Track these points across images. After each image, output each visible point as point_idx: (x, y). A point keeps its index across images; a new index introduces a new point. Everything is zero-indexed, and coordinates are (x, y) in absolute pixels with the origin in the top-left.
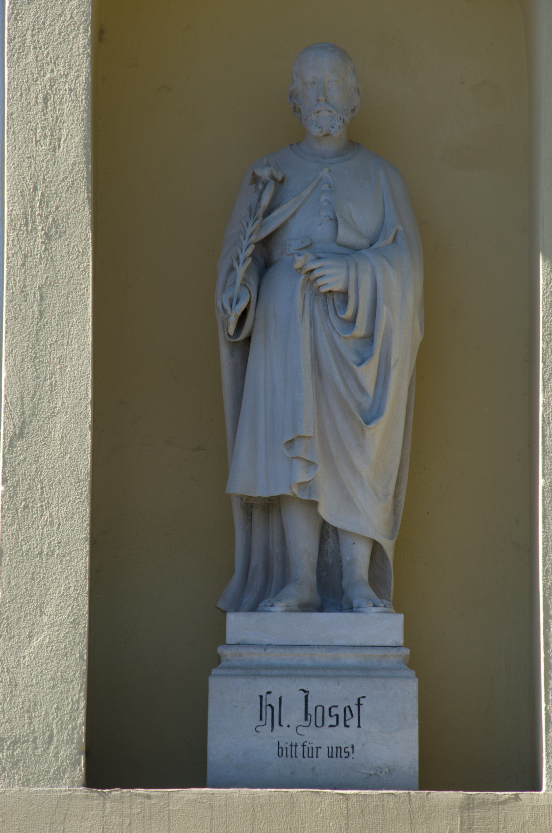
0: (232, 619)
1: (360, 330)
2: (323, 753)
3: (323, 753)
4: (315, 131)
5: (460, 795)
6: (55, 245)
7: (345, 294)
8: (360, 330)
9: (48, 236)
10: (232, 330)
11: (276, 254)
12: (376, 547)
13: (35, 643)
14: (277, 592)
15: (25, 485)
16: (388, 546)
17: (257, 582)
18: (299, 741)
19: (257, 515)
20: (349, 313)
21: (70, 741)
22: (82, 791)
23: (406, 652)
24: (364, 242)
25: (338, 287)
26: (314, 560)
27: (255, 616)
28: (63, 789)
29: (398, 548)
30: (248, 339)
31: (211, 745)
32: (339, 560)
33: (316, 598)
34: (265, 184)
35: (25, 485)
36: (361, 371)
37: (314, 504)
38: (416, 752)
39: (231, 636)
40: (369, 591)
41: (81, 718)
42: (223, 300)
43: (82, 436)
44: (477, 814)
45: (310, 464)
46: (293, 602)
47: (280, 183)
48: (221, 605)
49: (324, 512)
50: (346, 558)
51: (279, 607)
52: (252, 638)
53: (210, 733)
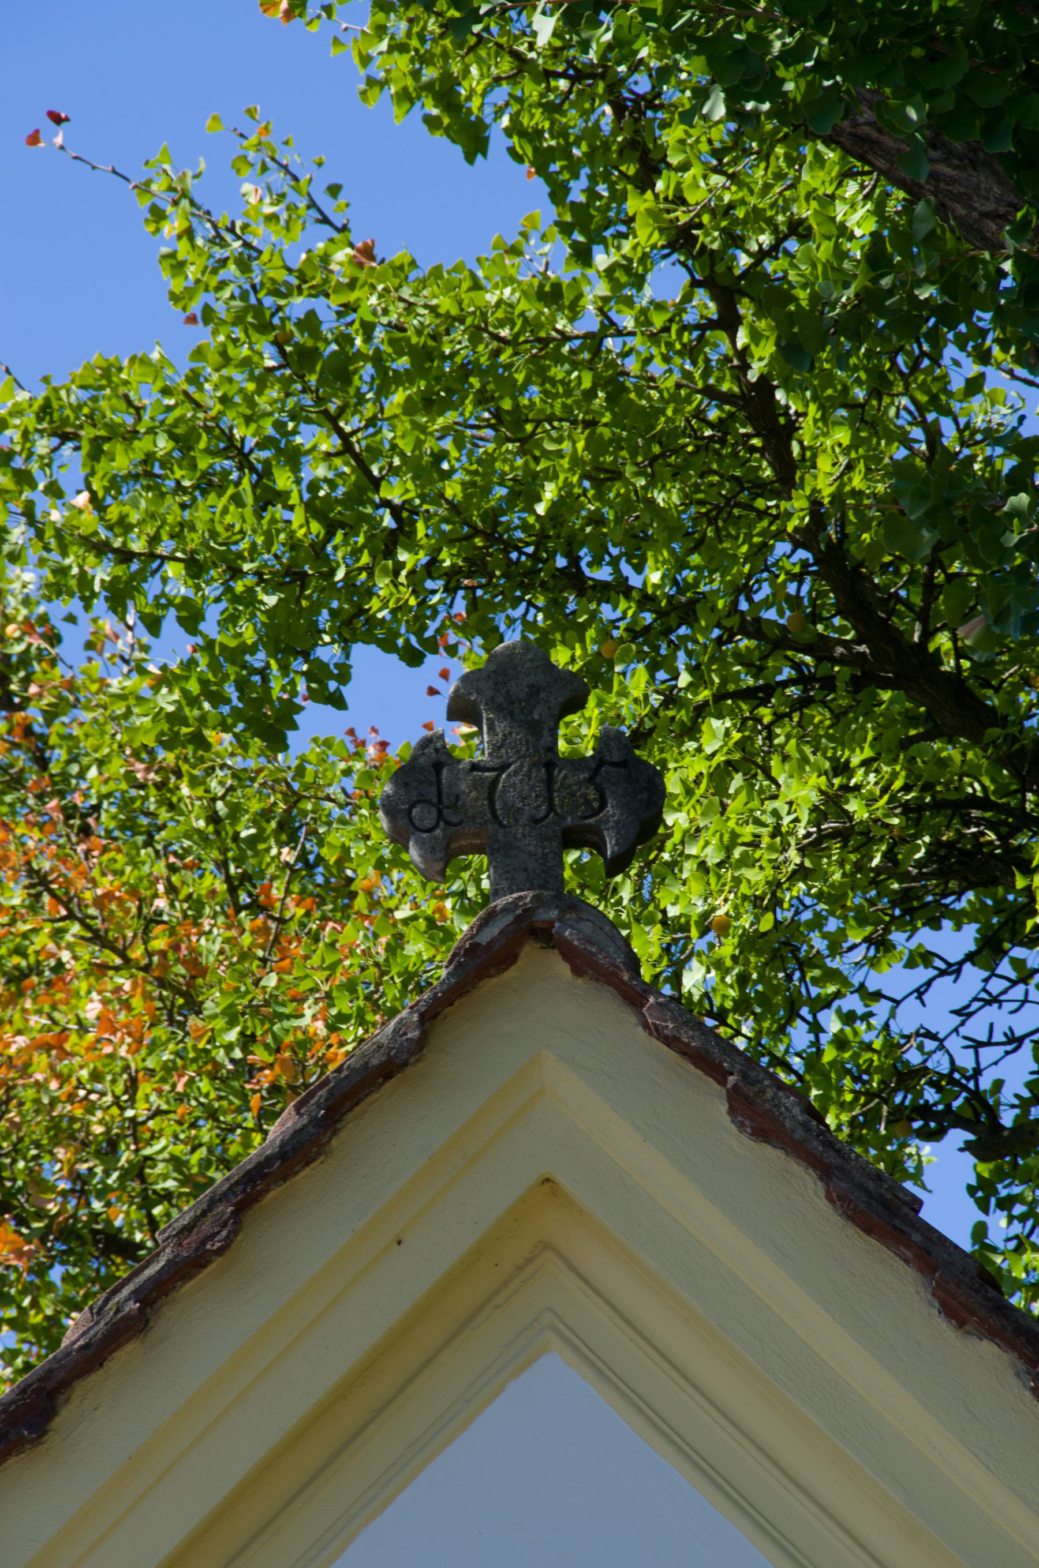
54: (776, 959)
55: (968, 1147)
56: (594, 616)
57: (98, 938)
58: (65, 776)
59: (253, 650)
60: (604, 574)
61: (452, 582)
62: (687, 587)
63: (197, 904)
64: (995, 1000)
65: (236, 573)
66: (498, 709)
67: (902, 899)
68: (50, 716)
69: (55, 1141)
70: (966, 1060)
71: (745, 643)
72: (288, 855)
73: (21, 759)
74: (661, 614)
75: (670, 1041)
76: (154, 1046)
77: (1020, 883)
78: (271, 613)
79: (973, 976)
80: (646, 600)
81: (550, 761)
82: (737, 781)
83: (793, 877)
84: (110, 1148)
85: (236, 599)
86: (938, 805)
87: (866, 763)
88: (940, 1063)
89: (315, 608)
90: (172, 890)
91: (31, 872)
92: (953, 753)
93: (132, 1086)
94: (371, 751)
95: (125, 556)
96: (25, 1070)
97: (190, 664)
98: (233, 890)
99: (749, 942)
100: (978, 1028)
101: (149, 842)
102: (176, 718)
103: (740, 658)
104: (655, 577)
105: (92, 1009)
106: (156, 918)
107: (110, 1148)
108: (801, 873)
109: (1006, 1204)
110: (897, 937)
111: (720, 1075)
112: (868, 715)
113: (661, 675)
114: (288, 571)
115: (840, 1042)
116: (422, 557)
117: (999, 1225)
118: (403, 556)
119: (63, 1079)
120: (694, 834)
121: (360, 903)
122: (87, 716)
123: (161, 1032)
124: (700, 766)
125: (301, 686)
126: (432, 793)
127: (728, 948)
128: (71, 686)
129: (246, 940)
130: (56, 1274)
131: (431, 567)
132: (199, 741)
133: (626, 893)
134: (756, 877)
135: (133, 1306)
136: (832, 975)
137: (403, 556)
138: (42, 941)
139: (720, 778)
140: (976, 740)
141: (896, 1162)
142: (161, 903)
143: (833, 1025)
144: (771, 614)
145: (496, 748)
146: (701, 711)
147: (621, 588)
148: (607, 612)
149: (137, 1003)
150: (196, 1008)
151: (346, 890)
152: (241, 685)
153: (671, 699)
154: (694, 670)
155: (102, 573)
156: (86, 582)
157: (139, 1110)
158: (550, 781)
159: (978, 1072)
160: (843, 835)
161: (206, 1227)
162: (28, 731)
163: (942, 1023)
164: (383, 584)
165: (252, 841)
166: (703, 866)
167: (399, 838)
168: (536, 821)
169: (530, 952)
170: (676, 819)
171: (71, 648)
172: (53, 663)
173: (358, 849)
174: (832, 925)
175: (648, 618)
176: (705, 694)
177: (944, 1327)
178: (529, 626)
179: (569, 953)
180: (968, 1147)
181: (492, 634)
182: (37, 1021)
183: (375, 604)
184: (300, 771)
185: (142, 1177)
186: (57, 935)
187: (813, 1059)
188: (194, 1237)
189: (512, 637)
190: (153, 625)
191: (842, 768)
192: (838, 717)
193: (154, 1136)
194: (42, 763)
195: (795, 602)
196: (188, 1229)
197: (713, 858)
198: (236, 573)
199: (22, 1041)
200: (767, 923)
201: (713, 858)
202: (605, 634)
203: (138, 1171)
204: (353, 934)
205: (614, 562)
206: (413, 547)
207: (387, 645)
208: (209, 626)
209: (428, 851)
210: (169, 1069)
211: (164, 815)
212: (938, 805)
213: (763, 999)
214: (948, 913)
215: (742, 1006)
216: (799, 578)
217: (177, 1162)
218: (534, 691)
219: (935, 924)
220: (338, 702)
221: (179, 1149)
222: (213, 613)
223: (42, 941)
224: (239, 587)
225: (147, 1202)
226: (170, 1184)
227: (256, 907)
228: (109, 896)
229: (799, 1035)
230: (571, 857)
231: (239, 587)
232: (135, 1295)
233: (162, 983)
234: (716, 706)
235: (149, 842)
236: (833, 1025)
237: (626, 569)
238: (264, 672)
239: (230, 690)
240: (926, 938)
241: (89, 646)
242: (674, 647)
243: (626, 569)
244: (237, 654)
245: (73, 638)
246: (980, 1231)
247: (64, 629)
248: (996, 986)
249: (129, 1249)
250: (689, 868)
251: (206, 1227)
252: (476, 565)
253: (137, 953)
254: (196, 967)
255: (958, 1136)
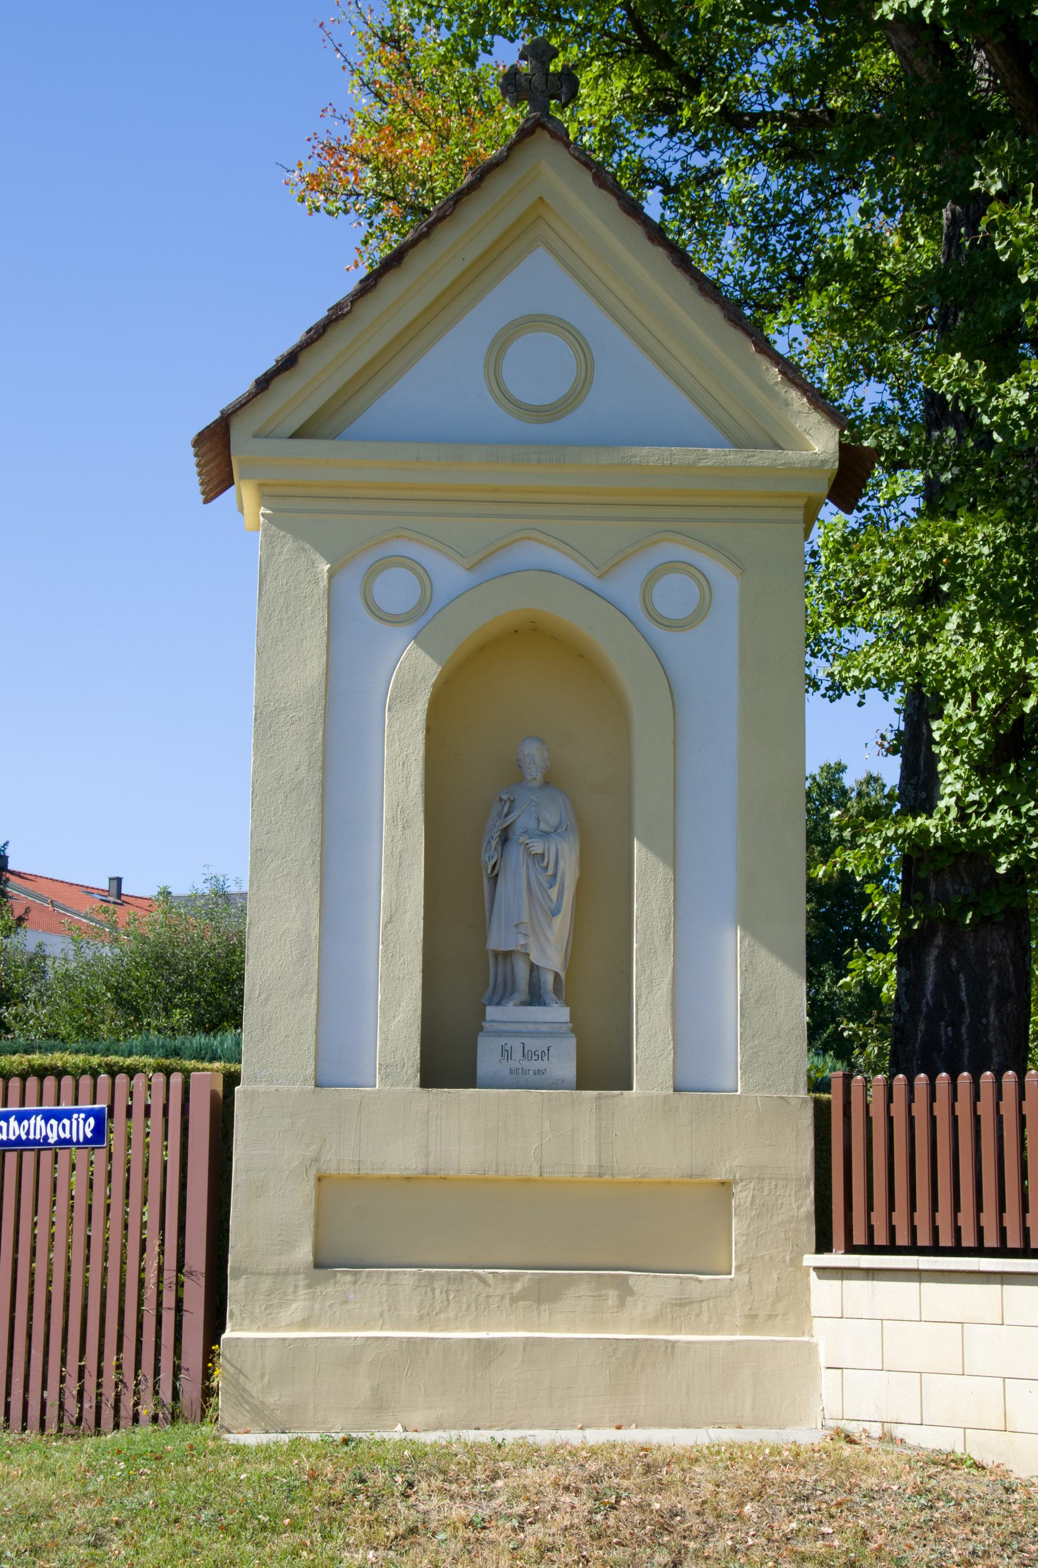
0: (488, 1008)
1: (550, 872)
2: (531, 1072)
3: (531, 1072)
4: (529, 777)
5: (596, 1092)
6: (407, 832)
7: (543, 855)
8: (550, 872)
9: (404, 828)
10: (489, 871)
11: (510, 835)
12: (557, 975)
13: (397, 1020)
14: (510, 995)
15: (392, 945)
16: (562, 974)
17: (500, 989)
18: (520, 1067)
19: (500, 958)
20: (545, 864)
21: (413, 1066)
22: (419, 1089)
23: (571, 1025)
24: (552, 830)
25: (540, 851)
26: (527, 981)
27: (499, 1008)
28: (410, 1088)
29: (566, 974)
30: (497, 875)
31: (478, 1068)
32: (539, 981)
33: (528, 998)
34: (505, 802)
35: (392, 945)
36: (550, 891)
37: (528, 954)
38: (575, 1072)
39: (488, 1018)
40: (553, 996)
41: (418, 1056)
42: (485, 857)
43: (418, 923)
44: (604, 1102)
45: (526, 935)
46: (518, 1001)
47: (512, 801)
48: (484, 1001)
49: (532, 958)
50: (543, 980)
51: (511, 1004)
52: (499, 1018)
53: (478, 1063)
54: (610, 135)
55: (661, 191)
56: (563, 29)
57: (422, 121)
58: (415, 72)
59: (466, 36)
60: (567, 16)
61: (524, 17)
62: (589, 22)
63: (450, 112)
64: (670, 148)
65: (462, 13)
66: (533, 57)
67: (647, 117)
68: (411, 54)
69: (409, 180)
70: (662, 166)
71: (606, 39)
72: (476, 99)
73: (403, 66)
74: (582, 29)
75: (577, 158)
76: (437, 154)
77: (679, 113)
78: (472, 25)
79: (666, 140)
80: (578, 25)
81: (547, 73)
82: (601, 80)
83: (616, 110)
84: (423, 184)
85: (462, 20)
86: (658, 90)
87: (638, 77)
88: (655, 167)
89: (485, 23)
90: (443, 108)
91: (404, 101)
92: (663, 74)
93: (430, 165)
94: (501, 68)
95: (431, 6)
96: (401, 160)
97: (449, 40)
98: (461, 109)
99: (603, 129)
100: (665, 157)
101: (438, 93)
102: (444, 56)
103: (605, 43)
104: (580, 18)
105: (420, 142)
106: (438, 117)
107: (423, 184)
108: (618, 109)
109: (670, 208)
110: (646, 129)
111: (590, 168)
112: (640, 62)
113: (582, 48)
114: (477, 12)
115: (627, 160)
116: (515, 9)
117: (668, 214)
118: (510, 9)
119: (411, 162)
120: (588, 96)
121: (496, 114)
122: (421, 54)
123: (439, 150)
124: (591, 75)
125: (479, 48)
126: (513, 82)
127: (596, 130)
128: (417, 45)
129: (464, 124)
130: (409, 218)
131: (518, 13)
132: (451, 64)
133: (568, 113)
134: (605, 109)
135: (425, 229)
136: (626, 140)
137: (510, 9)
138: (407, 122)
139: (596, 79)
140: (669, 70)
141: (641, 197)
142: (440, 112)
143: (625, 155)
144: (614, 30)
145: (532, 69)
146: (592, 59)
147: (571, 21)
148: (567, 28)
149: (433, 141)
150: (447, 142)
151: (491, 109)
152: (463, 47)
153: (584, 55)
154: (592, 47)
155: (424, 11)
156: (419, 13)
157: (433, 173)
158: (547, 79)
159: (665, 170)
160: (631, 98)
161: (446, 208)
162: (405, 58)
163: (656, 155)
164: (504, 17)
165: (465, 94)
166: (590, 105)
167: (504, 94)
168: (542, 91)
169: (539, 132)
170: (583, 91)
171: (417, 34)
172: (413, 37)
173: (493, 97)
174: (627, 125)
175: (579, 30)
176: (594, 54)
177: (648, 243)
178: (545, 32)
179: (550, 132)
180: (661, 191)
181: (534, 33)
182: (405, 145)
183: (501, 23)
184: (479, 73)
185: (432, 192)
186: (411, 120)
187: (619, 165)
188: (442, 211)
189: (541, 35)
190: (438, 27)
191: (632, 78)
192: (632, 62)
193: (436, 180)
194: (409, 68)
195: (621, 27)
196: (441, 208)
197: (593, 103)
198: (462, 13)
199: (400, 151)
200: (607, 123)
201: (593, 103)
202: (567, 34)
203: (432, 190)
204: (491, 122)
205: (570, 13)
206: (512, 6)
207: (505, 36)
208: (454, 29)
209: (512, 100)
210: (441, 161)
211: (442, 85)
212: (658, 90)
213: (606, 147)
214: (660, 122)
215: (600, 148)
216: (622, 20)
217: (443, 189)
218: (544, 51)
219: (657, 126)
220: (490, 53)
221: (443, 185)
222: (455, 24)
223: (407, 122)
224: (463, 17)
225: (434, 200)
226: (440, 194)
227: (467, 114)
228: (425, 109)
229: (616, 157)
230: (553, 102)
231: (463, 17)
232: (426, 226)
233: (440, 135)
234: (597, 58)
235: (438, 93)
236: (625, 155)
237: (573, 15)
238: (469, 43)
239: (460, 48)
240: (655, 130)
241: (423, 33)
242: (586, 39)
243: (573, 15)
244: (462, 37)
245: (419, 30)
246: (662, 216)
247: (416, 27)
248: (671, 144)
249: (429, 213)
250: (586, 106)
251: (446, 208)
252: (530, 13)
253: (433, 126)
254: (449, 130)
255: (658, 188)
